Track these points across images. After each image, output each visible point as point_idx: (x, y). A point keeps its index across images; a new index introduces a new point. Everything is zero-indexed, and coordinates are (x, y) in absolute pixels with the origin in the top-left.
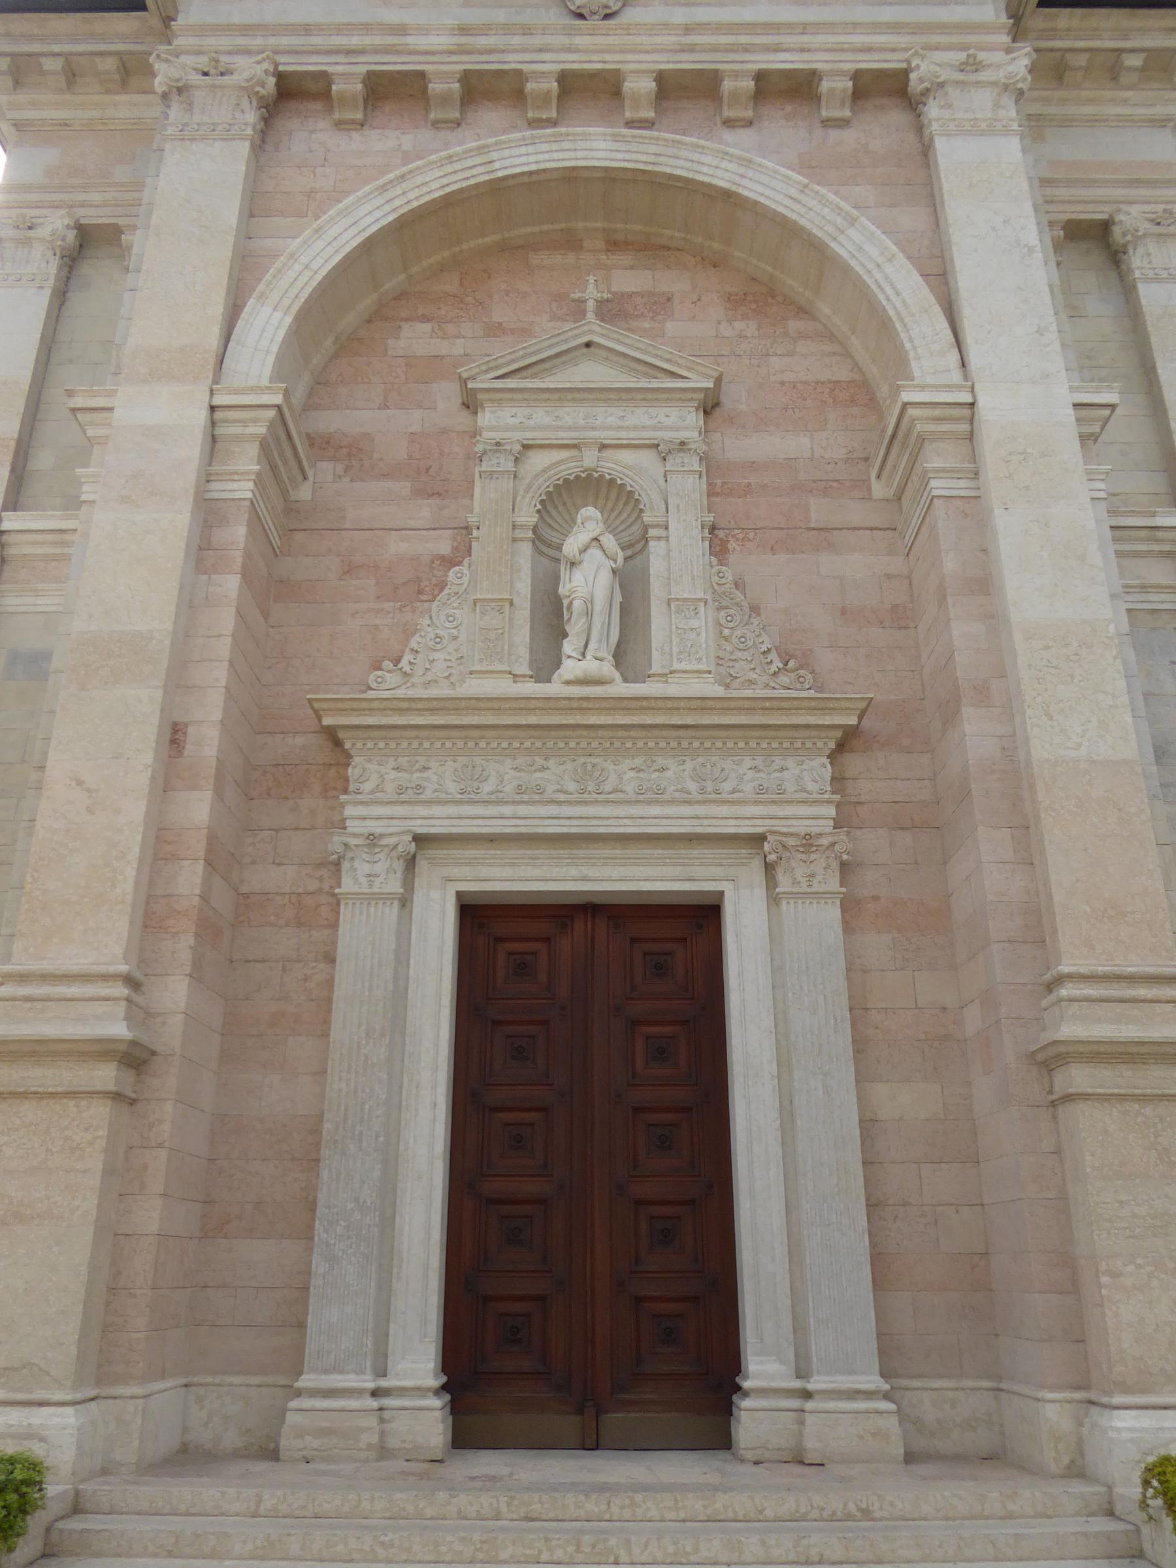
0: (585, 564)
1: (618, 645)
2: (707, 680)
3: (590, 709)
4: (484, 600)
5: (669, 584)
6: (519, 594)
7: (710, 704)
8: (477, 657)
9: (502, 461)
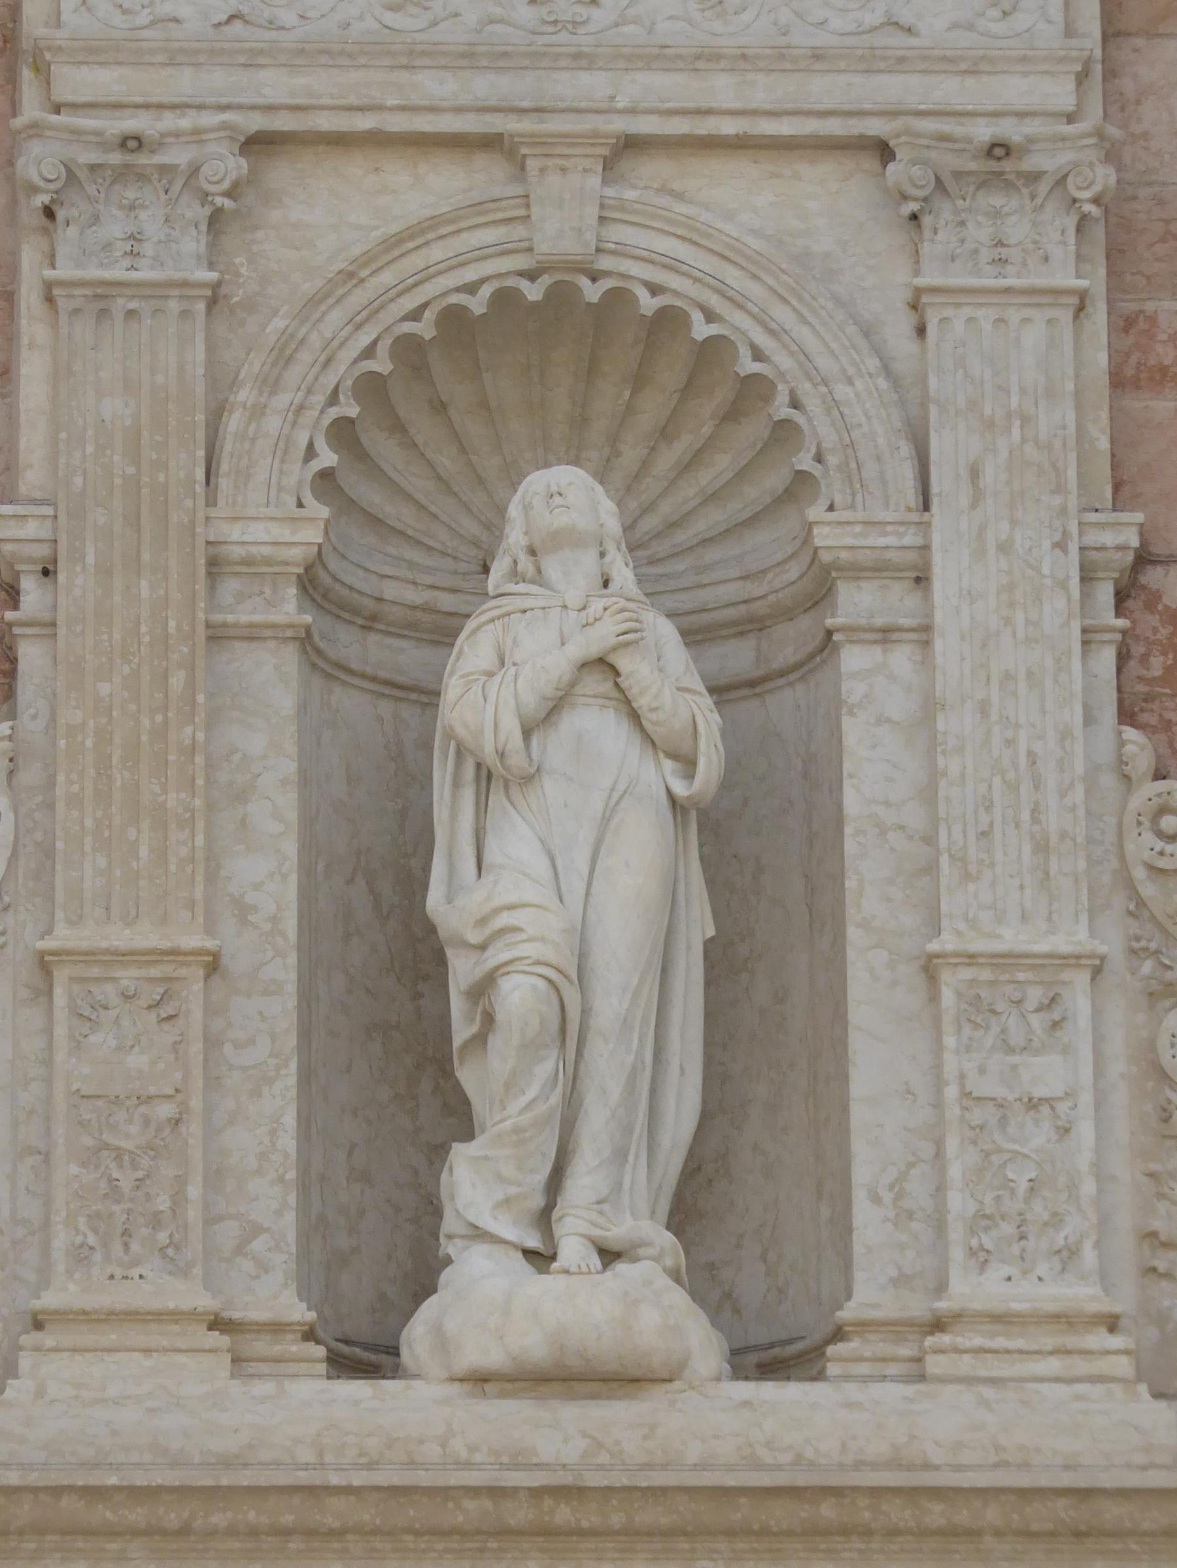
0: (550, 787)
1: (692, 1171)
2: (1102, 1366)
3: (581, 1533)
4: (90, 956)
5: (931, 869)
6: (243, 911)
7: (1113, 1512)
8: (61, 1240)
9: (151, 222)
